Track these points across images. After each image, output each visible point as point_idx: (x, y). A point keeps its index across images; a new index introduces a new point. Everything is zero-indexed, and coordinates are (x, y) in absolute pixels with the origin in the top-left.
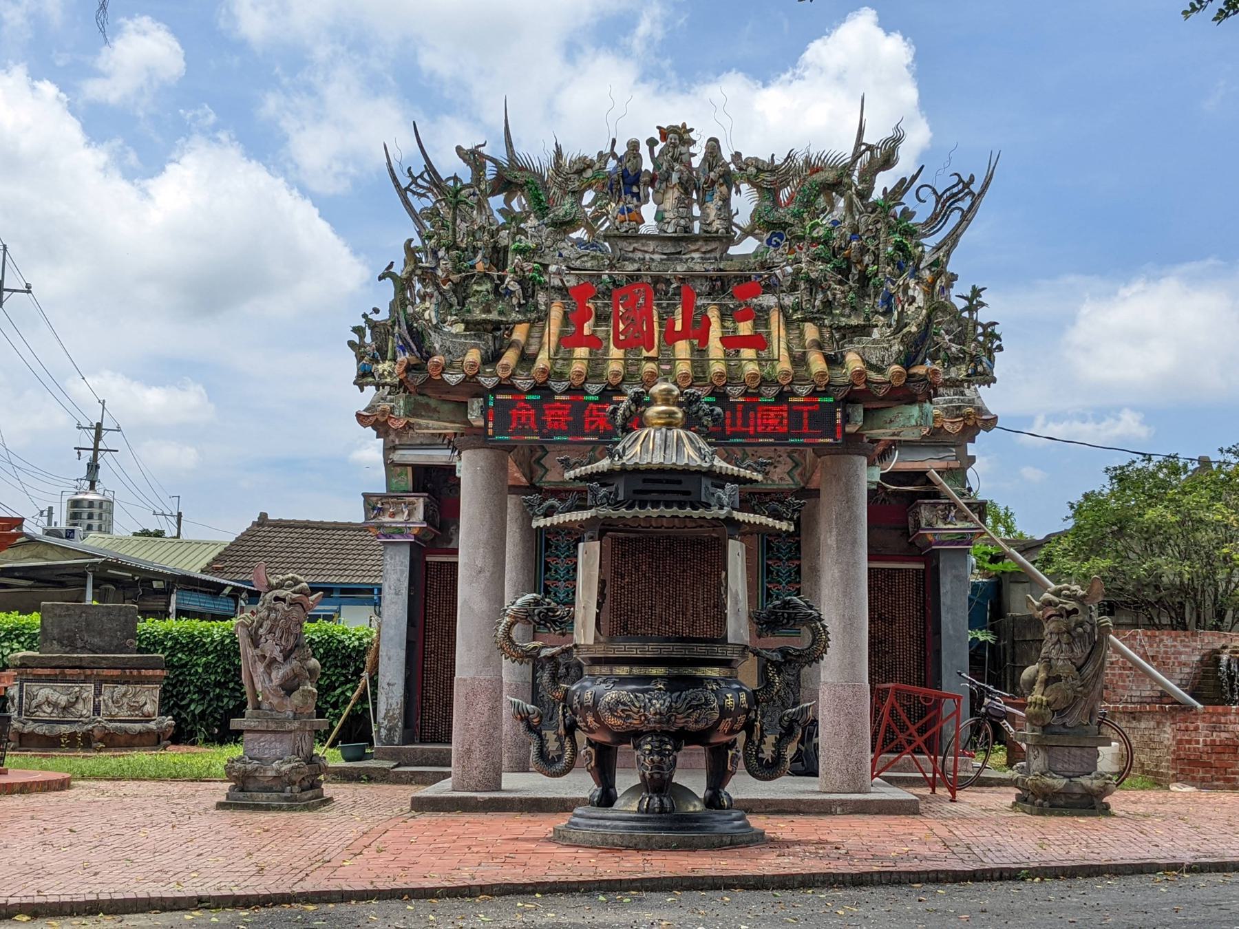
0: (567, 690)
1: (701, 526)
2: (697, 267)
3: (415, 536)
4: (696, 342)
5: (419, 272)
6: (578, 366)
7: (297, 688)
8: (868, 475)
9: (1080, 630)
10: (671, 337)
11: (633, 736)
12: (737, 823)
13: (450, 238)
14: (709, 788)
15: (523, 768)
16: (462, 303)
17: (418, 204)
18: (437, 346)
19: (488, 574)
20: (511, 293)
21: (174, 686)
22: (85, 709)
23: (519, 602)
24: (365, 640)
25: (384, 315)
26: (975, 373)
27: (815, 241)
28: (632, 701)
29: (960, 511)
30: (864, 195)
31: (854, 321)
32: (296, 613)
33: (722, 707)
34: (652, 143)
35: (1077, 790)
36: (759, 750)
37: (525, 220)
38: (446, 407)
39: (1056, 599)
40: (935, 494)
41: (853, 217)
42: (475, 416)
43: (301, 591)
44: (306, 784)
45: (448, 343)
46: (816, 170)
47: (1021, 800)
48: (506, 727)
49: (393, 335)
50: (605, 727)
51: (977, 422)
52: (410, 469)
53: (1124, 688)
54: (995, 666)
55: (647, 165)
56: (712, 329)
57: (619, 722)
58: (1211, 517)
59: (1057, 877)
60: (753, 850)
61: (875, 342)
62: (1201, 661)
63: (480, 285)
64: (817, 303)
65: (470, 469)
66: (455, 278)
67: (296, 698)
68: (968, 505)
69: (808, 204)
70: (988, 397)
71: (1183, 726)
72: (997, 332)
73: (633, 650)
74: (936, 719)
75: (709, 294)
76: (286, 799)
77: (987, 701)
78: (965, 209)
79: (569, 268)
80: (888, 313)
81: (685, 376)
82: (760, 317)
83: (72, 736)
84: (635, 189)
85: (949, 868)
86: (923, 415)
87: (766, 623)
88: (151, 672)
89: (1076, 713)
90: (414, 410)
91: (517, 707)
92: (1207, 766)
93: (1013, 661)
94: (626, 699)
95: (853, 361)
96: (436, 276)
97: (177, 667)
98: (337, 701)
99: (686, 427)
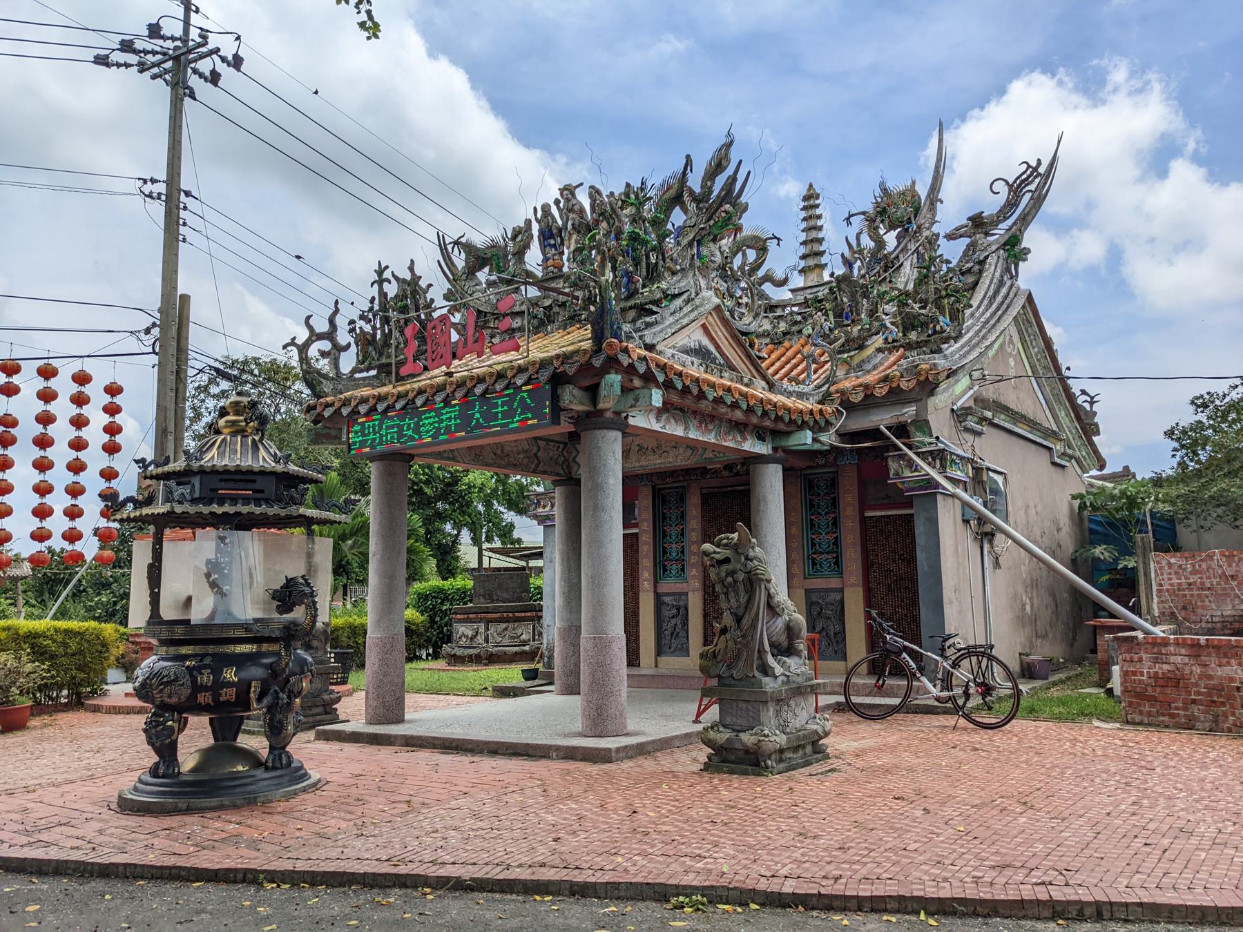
9: (730, 579)
22: (480, 639)
35: (738, 746)
53: (1204, 607)
71: (1128, 656)
84: (552, 242)
92: (1152, 699)
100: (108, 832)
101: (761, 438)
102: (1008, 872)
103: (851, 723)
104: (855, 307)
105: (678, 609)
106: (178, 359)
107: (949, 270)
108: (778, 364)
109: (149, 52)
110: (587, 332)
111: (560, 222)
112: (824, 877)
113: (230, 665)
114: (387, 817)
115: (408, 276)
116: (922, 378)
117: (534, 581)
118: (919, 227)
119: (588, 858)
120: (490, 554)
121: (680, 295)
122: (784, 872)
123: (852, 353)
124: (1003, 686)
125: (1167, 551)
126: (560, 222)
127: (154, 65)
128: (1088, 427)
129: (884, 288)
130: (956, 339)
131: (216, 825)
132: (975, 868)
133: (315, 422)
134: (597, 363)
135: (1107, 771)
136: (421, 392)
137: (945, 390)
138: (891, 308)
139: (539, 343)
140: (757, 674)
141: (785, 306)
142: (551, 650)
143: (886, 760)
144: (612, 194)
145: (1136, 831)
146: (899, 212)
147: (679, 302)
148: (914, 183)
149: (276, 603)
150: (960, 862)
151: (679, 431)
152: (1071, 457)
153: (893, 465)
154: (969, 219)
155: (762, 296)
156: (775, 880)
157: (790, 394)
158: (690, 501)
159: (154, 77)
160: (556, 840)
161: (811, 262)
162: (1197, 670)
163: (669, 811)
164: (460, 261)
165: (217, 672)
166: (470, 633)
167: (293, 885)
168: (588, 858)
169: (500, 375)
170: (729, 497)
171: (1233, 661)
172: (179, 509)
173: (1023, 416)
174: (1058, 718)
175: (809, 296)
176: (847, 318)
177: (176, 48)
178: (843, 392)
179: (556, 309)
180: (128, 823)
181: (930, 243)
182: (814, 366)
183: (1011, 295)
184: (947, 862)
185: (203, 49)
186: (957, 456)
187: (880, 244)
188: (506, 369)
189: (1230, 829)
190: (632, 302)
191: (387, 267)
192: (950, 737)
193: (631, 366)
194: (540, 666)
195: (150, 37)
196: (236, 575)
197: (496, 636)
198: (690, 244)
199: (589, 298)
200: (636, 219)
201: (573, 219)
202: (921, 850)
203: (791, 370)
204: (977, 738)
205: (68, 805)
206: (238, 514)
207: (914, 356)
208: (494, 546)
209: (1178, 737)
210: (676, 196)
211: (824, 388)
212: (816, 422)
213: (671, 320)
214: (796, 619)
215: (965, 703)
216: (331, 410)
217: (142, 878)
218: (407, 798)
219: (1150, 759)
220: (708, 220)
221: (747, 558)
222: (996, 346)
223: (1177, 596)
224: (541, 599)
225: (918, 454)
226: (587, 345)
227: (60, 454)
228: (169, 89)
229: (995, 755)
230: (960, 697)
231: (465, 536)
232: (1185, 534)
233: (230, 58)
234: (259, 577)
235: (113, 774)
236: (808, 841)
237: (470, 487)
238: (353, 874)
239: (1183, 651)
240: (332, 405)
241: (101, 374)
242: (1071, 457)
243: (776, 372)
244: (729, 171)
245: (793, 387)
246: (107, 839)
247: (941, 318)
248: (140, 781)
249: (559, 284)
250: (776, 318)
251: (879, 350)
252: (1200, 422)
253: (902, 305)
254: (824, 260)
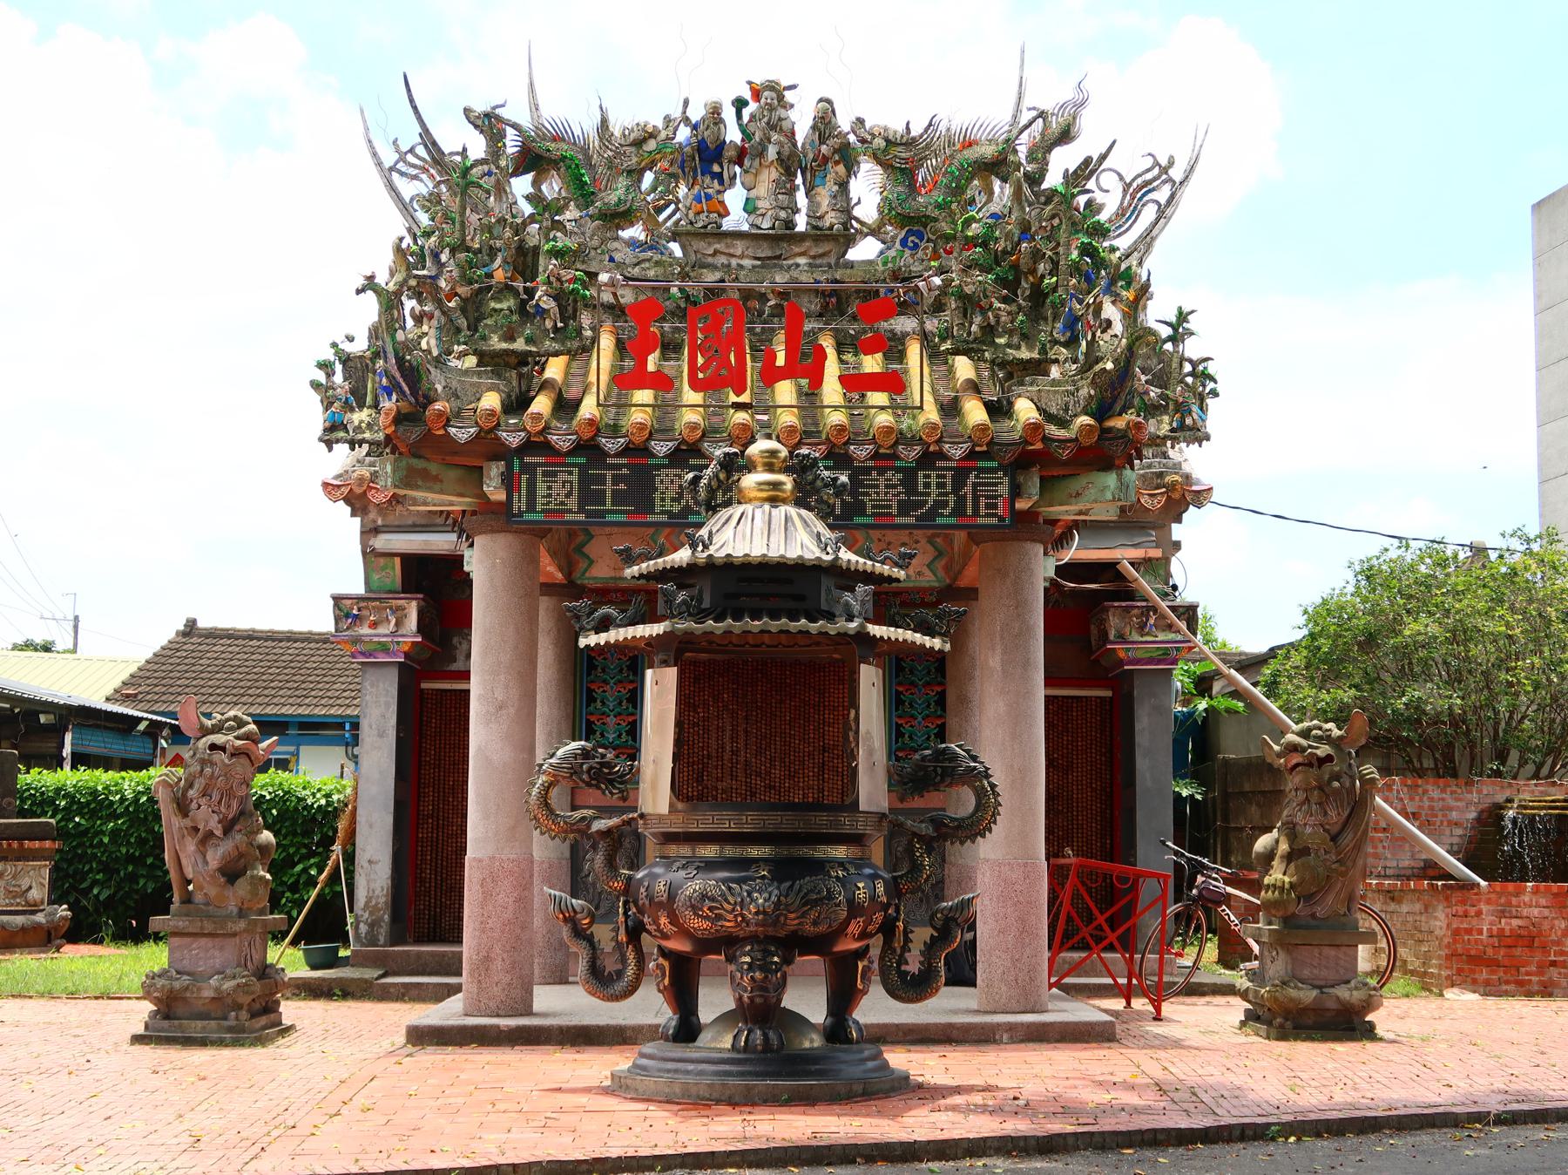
0: (630, 878)
1: (818, 644)
2: (804, 278)
3: (406, 655)
4: (804, 382)
5: (413, 283)
6: (638, 416)
7: (242, 873)
8: (1044, 567)
9: (1336, 784)
10: (771, 376)
11: (726, 944)
12: (870, 1064)
13: (457, 235)
14: (830, 1013)
15: (560, 977)
16: (473, 328)
17: (408, 189)
18: (439, 388)
19: (512, 711)
20: (542, 313)
21: (70, 862)
23: (560, 753)
24: (335, 797)
25: (360, 346)
26: (1183, 427)
27: (970, 243)
28: (723, 895)
29: (1163, 617)
30: (1035, 179)
31: (1025, 354)
32: (241, 766)
33: (851, 902)
34: (740, 104)
35: (1332, 1005)
36: (902, 960)
37: (560, 211)
38: (452, 474)
39: (1304, 742)
40: (1126, 592)
41: (1023, 209)
42: (494, 491)
43: (247, 737)
44: (257, 1006)
45: (454, 384)
46: (969, 144)
47: (1251, 1017)
48: (537, 921)
49: (374, 372)
50: (685, 933)
51: (1183, 496)
52: (397, 560)
53: (1376, 856)
54: (1202, 829)
55: (733, 135)
56: (827, 363)
57: (706, 924)
58: (1490, 626)
59: (1319, 1135)
60: (895, 1102)
61: (1054, 383)
62: (1478, 820)
63: (500, 301)
64: (974, 328)
65: (483, 562)
66: (463, 290)
67: (242, 887)
68: (1173, 609)
69: (958, 191)
70: (1193, 460)
71: (1460, 909)
72: (1211, 371)
73: (726, 822)
74: (1131, 910)
75: (821, 315)
76: (230, 1030)
77: (1200, 879)
78: (1163, 202)
79: (627, 278)
80: (1072, 343)
81: (791, 430)
82: (893, 348)
84: (716, 168)
85: (1171, 1125)
86: (1123, 486)
87: (911, 781)
88: (37, 844)
89: (1330, 899)
90: (409, 479)
91: (558, 902)
92: (1492, 964)
93: (1225, 819)
94: (716, 892)
95: (1025, 410)
96: (438, 288)
97: (74, 836)
98: (297, 881)
99: (800, 503)
201: (779, 143)
239: (1543, 902)
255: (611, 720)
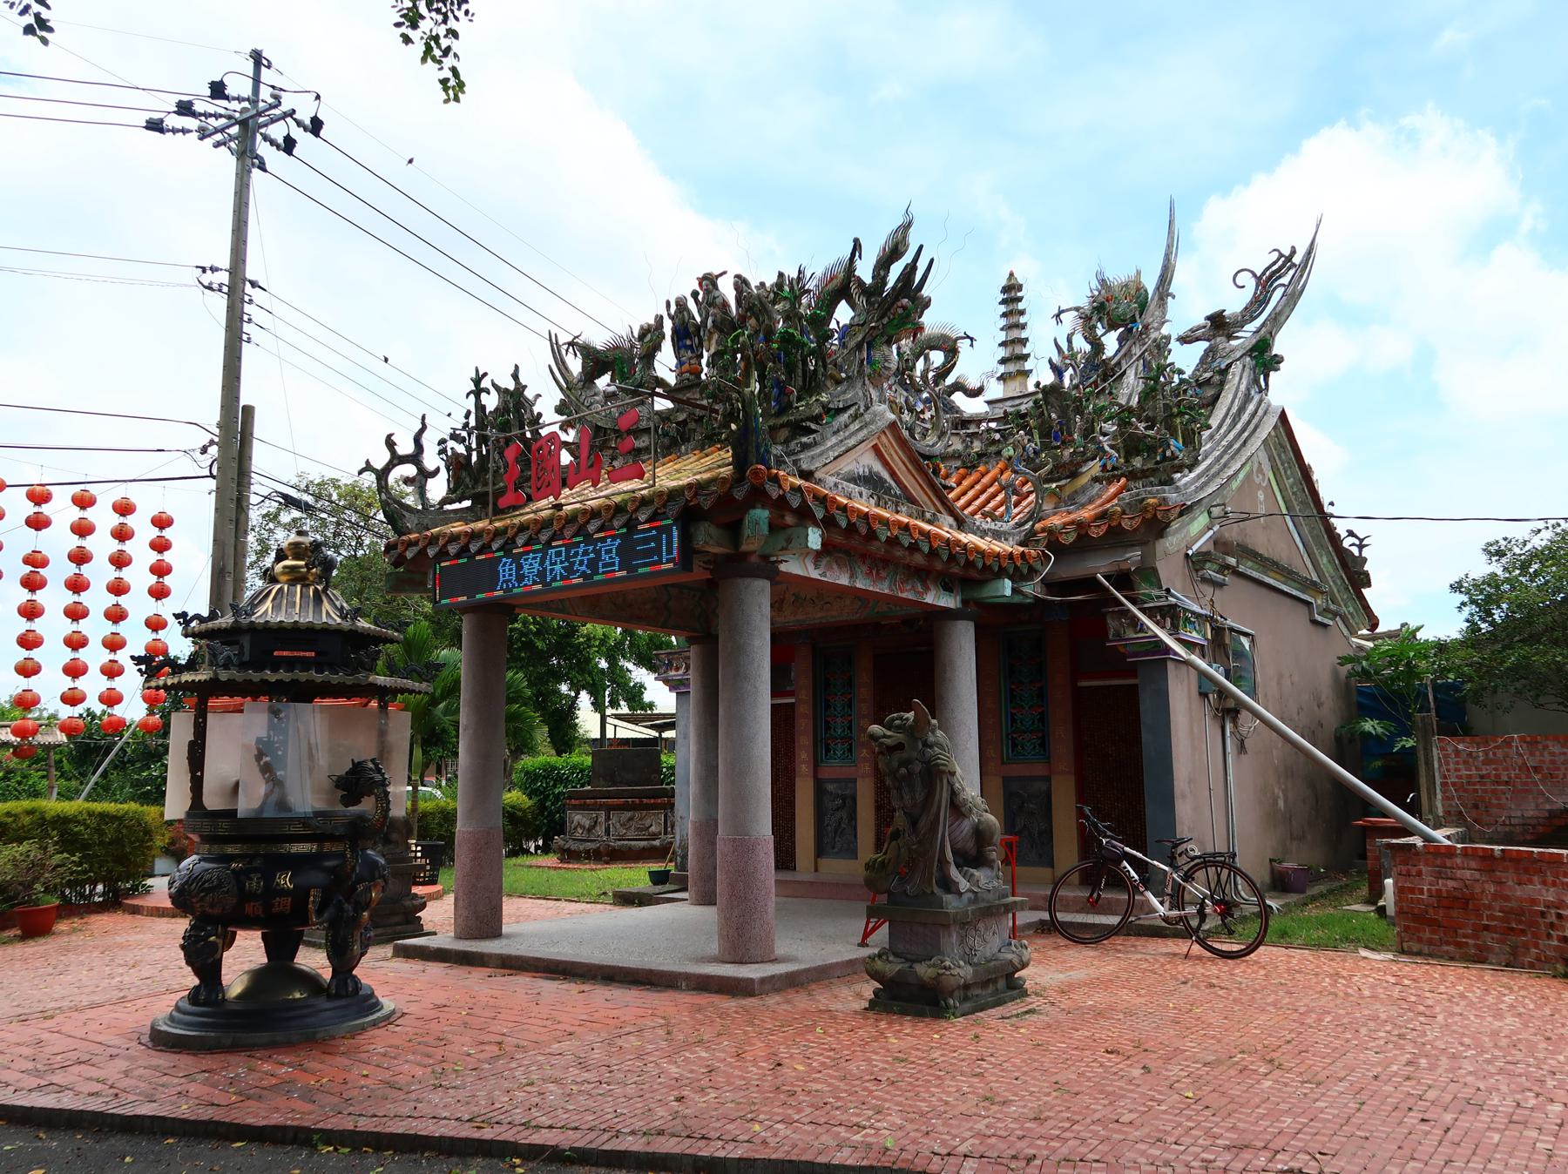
9: (903, 770)
22: (600, 830)
53: (1500, 806)
71: (1404, 868)
83: (587, 852)
92: (1433, 924)
100: (136, 1073)
101: (948, 589)
102: (1246, 1155)
103: (1057, 948)
104: (1066, 424)
105: (844, 799)
106: (239, 484)
107: (1182, 381)
108: (971, 494)
109: (211, 115)
110: (727, 455)
111: (698, 319)
112: (1014, 1157)
113: (284, 869)
114: (472, 1063)
115: (511, 386)
116: (1149, 516)
117: (666, 759)
118: (1146, 327)
119: (718, 1125)
120: (617, 722)
121: (849, 407)
122: (963, 1149)
123: (1063, 482)
124: (1247, 900)
125: (1453, 734)
126: (698, 319)
127: (217, 131)
128: (1355, 575)
129: (1102, 402)
130: (1191, 468)
131: (266, 1067)
132: (1205, 1149)
133: (396, 564)
134: (739, 494)
135: (1375, 1018)
136: (522, 528)
137: (1177, 530)
138: (1110, 427)
139: (670, 467)
140: (936, 890)
141: (980, 421)
142: (685, 848)
143: (1095, 999)
144: (762, 284)
145: (1411, 1101)
146: (1121, 310)
147: (844, 417)
148: (1139, 273)
149: (340, 793)
150: (1187, 1140)
151: (844, 580)
152: (1335, 614)
153: (1112, 624)
154: (1208, 318)
155: (952, 408)
156: (952, 1160)
157: (983, 534)
158: (858, 667)
159: (217, 145)
160: (680, 1099)
161: (1012, 368)
162: (1492, 888)
163: (823, 1064)
164: (575, 365)
165: (269, 877)
166: (587, 823)
167: (353, 1149)
168: (718, 1125)
169: (619, 509)
170: (901, 662)
171: (1536, 878)
172: (224, 676)
173: (1275, 563)
174: (1317, 946)
175: (1009, 410)
176: (1056, 439)
177: (244, 110)
178: (1050, 531)
179: (692, 425)
180: (161, 1062)
181: (1158, 347)
182: (1014, 498)
183: (1260, 412)
184: (1170, 1139)
185: (276, 112)
186: (1193, 613)
187: (1098, 347)
188: (625, 502)
189: (1532, 1102)
190: (784, 419)
191: (485, 374)
192: (1180, 968)
193: (782, 498)
194: (671, 867)
195: (212, 97)
196: (291, 757)
197: (617, 828)
198: (859, 347)
199: (731, 413)
200: (791, 316)
201: (714, 315)
202: (1138, 1122)
203: (988, 501)
204: (1214, 970)
205: (91, 1036)
206: (295, 682)
207: (1138, 488)
208: (620, 711)
209: (1466, 973)
210: (842, 286)
211: (1027, 526)
212: (1016, 568)
213: (834, 440)
214: (987, 821)
215: (1200, 926)
216: (415, 549)
217: (172, 1135)
218: (499, 1039)
219: (1430, 1002)
220: (882, 317)
221: (926, 745)
222: (1241, 476)
223: (1466, 791)
224: (673, 782)
225: (1143, 610)
226: (726, 471)
227: (97, 599)
228: (234, 159)
229: (1235, 994)
230: (1193, 916)
231: (585, 699)
232: (1476, 715)
233: (308, 122)
234: (323, 760)
235: (149, 996)
236: (996, 1108)
237: (589, 639)
238: (426, 1137)
239: (1473, 864)
240: (416, 543)
241: (148, 502)
242: (1335, 614)
243: (969, 504)
244: (907, 258)
245: (989, 524)
246: (133, 1082)
247: (1172, 442)
248: (177, 1008)
249: (694, 395)
250: (968, 435)
251: (1096, 480)
252: (1494, 575)
253: (1124, 424)
254: (1028, 365)
255: (839, 720)
